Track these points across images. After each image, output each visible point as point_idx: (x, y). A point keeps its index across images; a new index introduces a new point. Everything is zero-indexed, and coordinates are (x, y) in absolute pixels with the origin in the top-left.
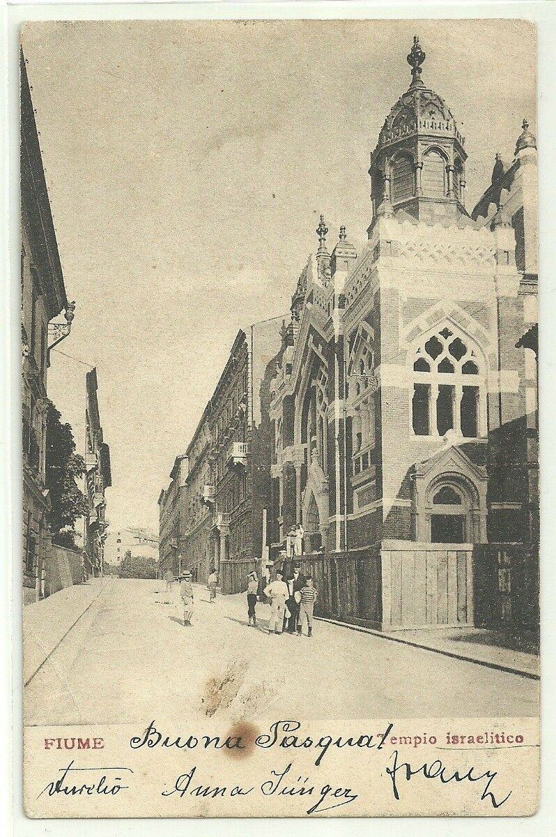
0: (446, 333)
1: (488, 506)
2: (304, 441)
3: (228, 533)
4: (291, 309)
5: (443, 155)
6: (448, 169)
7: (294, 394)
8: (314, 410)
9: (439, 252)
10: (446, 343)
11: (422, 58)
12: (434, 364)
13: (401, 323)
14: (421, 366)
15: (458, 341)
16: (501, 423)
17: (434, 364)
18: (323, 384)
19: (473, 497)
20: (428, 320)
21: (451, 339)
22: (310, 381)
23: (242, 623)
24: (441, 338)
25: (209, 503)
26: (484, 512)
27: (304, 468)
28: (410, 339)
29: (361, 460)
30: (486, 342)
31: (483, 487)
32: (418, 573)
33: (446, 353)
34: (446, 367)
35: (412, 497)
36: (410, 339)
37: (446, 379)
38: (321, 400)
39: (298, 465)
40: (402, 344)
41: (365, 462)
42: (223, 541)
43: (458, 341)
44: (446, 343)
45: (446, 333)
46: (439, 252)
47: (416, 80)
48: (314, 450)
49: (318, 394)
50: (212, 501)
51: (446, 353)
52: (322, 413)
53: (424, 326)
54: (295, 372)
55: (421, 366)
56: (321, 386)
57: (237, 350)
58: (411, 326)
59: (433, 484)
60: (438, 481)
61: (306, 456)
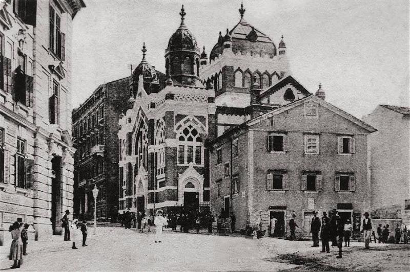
0: (190, 127)
2: (136, 154)
7: (132, 132)
8: (141, 143)
9: (188, 97)
10: (190, 130)
12: (186, 138)
13: (174, 123)
15: (194, 129)
16: (269, 99)
17: (186, 138)
18: (146, 131)
21: (192, 129)
22: (139, 130)
24: (188, 129)
27: (136, 166)
28: (178, 129)
29: (175, 119)
32: (132, 226)
33: (190, 134)
34: (190, 139)
35: (177, 186)
36: (178, 129)
37: (190, 143)
38: (144, 139)
39: (133, 164)
40: (175, 131)
41: (162, 171)
43: (194, 129)
44: (190, 130)
45: (190, 127)
48: (141, 160)
49: (143, 135)
51: (190, 134)
52: (145, 144)
53: (183, 124)
54: (133, 123)
55: (182, 139)
56: (145, 132)
61: (137, 161)
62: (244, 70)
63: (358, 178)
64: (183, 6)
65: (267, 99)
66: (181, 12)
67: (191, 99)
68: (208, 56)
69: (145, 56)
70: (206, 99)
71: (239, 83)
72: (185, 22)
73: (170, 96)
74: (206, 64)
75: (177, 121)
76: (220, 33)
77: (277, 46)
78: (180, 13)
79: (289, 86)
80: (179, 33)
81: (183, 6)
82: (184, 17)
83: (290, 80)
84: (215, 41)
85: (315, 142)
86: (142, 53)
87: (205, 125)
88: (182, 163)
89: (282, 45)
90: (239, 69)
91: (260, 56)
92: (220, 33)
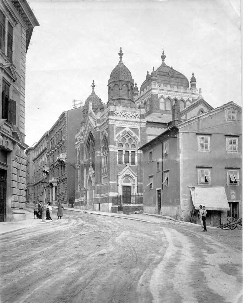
1: (137, 183)
3: (56, 185)
4: (83, 111)
5: (102, 237)
6: (129, 90)
11: (122, 54)
13: (115, 134)
14: (121, 145)
19: (133, 180)
20: (122, 133)
23: (204, 184)
25: (47, 173)
26: (136, 185)
30: (138, 140)
31: (136, 178)
42: (54, 188)
46: (125, 114)
47: (121, 61)
50: (48, 172)
57: (61, 118)
58: (118, 135)
59: (123, 177)
60: (125, 176)
62: (165, 97)
63: (240, 204)
64: (93, 81)
65: (185, 116)
66: (92, 84)
67: (131, 116)
68: (139, 90)
69: (95, 90)
70: (138, 116)
71: (162, 107)
72: (95, 90)
73: (165, 70)
74: (138, 95)
75: (117, 132)
76: (148, 72)
77: (189, 81)
78: (92, 86)
79: (201, 106)
80: (90, 97)
81: (93, 81)
82: (95, 88)
83: (202, 102)
84: (144, 79)
85: (235, 143)
86: (92, 88)
87: (138, 136)
88: (121, 164)
89: (193, 79)
90: (162, 97)
91: (177, 88)
92: (148, 72)
